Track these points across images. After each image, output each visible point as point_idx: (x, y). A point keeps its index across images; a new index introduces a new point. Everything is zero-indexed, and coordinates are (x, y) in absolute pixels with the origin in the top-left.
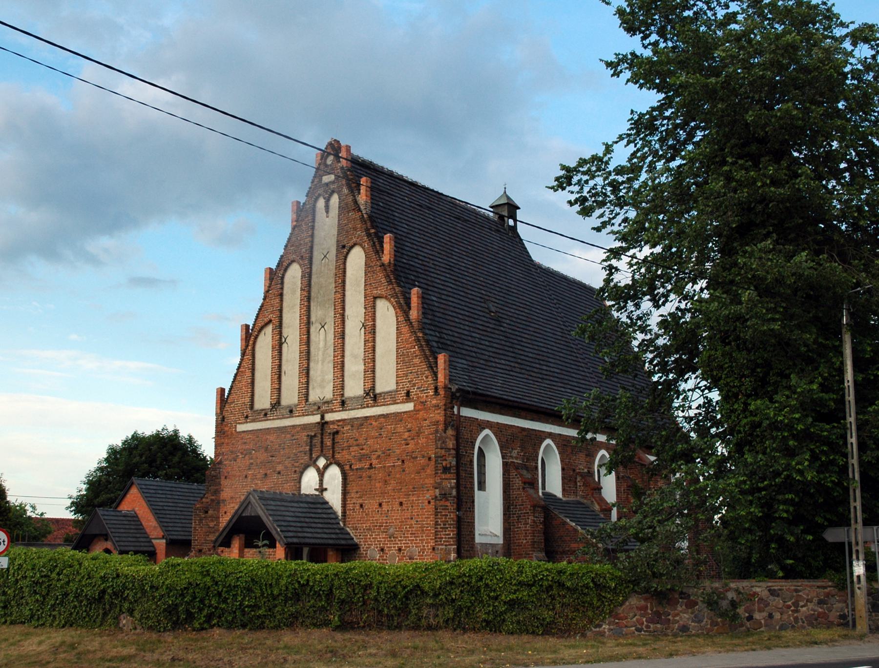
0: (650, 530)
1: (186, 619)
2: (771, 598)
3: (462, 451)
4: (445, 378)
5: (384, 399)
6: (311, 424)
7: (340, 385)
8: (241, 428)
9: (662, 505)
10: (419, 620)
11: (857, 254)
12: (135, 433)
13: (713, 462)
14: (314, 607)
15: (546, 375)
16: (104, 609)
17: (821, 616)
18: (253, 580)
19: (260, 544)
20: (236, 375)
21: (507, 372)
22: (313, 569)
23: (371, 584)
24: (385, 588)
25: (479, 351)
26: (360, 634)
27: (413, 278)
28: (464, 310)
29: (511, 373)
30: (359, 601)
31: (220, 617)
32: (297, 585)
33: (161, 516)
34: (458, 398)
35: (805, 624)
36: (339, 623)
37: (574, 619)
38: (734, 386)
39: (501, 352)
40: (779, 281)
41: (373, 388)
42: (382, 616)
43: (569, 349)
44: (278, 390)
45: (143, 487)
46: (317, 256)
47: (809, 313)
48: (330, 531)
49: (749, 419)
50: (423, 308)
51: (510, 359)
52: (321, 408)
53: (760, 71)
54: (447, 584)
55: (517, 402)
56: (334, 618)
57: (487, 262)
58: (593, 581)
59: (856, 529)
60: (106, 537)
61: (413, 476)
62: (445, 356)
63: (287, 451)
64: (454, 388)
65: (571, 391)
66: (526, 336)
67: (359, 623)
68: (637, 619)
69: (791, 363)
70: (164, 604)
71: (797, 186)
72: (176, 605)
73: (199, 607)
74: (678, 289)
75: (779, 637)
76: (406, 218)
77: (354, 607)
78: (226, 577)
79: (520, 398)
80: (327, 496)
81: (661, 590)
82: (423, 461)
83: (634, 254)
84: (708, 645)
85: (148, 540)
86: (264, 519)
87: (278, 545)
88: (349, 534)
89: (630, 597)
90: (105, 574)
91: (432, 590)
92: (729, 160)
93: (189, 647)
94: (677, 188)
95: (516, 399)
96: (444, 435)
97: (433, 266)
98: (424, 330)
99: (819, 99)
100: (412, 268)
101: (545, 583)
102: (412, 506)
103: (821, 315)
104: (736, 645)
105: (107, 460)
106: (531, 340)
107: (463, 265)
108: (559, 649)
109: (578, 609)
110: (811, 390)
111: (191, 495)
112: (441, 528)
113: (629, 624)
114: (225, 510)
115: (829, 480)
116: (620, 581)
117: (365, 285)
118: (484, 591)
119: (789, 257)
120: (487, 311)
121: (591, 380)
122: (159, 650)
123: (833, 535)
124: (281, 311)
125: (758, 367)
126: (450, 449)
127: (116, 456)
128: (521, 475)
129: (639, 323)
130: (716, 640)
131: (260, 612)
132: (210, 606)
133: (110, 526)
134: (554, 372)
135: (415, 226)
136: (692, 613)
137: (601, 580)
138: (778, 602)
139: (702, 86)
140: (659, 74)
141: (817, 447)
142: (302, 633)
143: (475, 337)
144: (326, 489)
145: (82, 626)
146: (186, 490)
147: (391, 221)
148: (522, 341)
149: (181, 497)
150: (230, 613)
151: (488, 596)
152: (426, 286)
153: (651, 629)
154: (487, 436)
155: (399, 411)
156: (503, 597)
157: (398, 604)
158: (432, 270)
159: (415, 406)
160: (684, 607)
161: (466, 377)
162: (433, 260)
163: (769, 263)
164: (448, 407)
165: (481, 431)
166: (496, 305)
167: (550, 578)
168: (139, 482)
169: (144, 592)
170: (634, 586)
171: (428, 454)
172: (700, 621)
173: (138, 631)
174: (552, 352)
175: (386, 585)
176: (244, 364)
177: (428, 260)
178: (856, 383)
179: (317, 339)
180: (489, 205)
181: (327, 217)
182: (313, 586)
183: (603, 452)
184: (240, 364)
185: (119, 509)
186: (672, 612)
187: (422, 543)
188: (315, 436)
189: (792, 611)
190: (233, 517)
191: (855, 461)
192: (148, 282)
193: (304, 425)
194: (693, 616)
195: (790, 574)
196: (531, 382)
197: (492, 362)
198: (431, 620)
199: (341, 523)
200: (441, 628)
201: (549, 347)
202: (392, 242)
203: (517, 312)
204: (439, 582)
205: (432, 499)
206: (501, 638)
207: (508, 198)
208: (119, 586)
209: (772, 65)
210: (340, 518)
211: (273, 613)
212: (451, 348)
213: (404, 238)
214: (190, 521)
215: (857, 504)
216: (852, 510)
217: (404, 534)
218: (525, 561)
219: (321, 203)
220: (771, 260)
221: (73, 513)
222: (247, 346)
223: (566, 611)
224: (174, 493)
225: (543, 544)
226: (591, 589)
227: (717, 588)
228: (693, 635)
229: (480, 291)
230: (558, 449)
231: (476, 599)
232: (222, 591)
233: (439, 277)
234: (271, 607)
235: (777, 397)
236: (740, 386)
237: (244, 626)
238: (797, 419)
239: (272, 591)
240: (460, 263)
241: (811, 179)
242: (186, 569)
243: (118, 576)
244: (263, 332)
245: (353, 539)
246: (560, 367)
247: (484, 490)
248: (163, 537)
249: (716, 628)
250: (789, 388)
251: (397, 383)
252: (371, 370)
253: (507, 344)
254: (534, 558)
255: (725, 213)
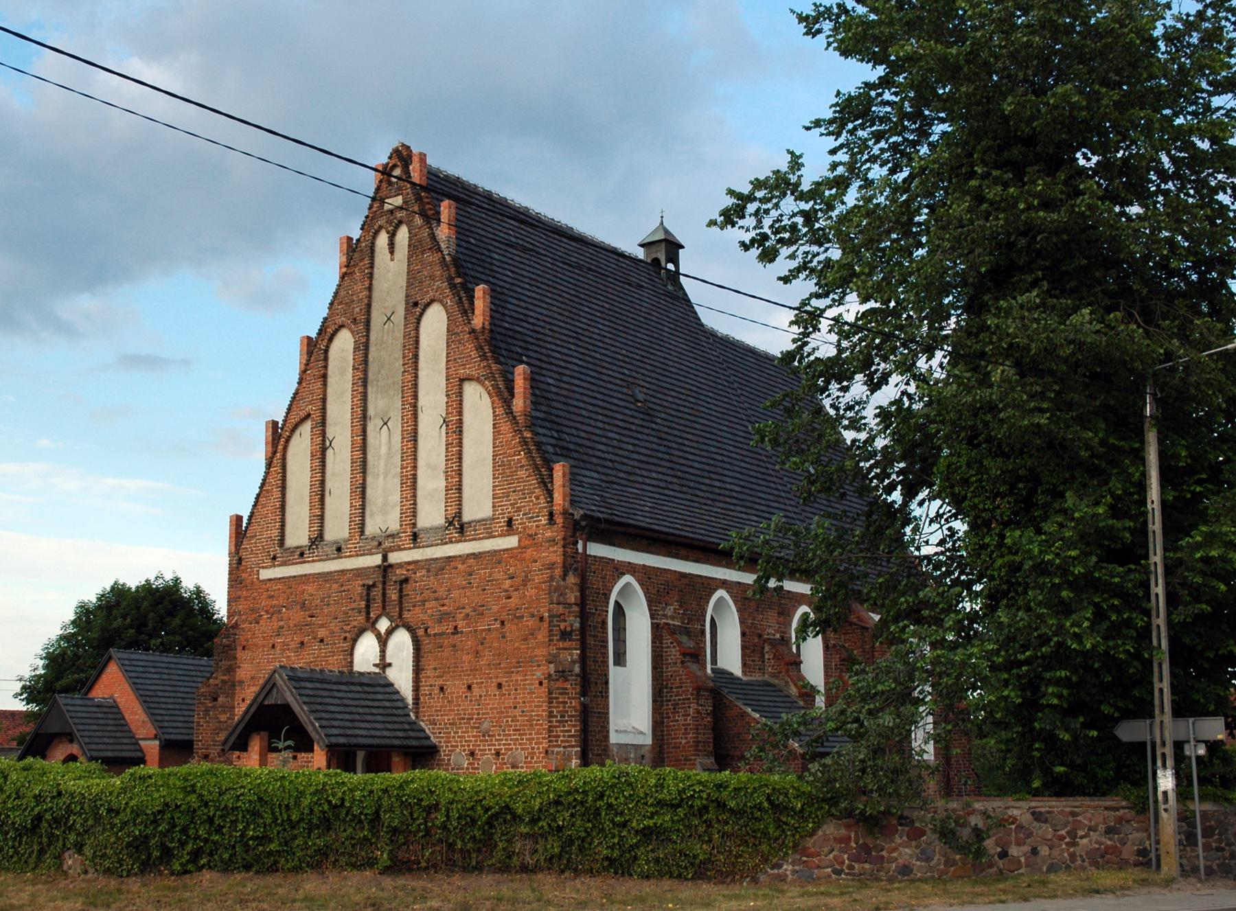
0: (855, 725)
1: (161, 857)
2: (1036, 824)
3: (590, 608)
4: (564, 500)
5: (475, 530)
6: (369, 568)
7: (411, 510)
8: (265, 574)
9: (875, 687)
10: (509, 857)
11: (1169, 311)
12: (116, 583)
13: (951, 623)
14: (352, 838)
15: (719, 495)
16: (40, 843)
17: (1110, 851)
18: (260, 799)
19: (281, 746)
20: (258, 496)
21: (661, 491)
22: (351, 783)
23: (437, 804)
24: (458, 810)
25: (617, 458)
26: (419, 879)
27: (519, 350)
28: (596, 398)
29: (667, 492)
30: (419, 830)
31: (211, 854)
32: (326, 807)
33: (152, 705)
34: (583, 528)
35: (1086, 864)
36: (389, 863)
37: (741, 856)
38: (985, 510)
39: (651, 460)
40: (1050, 351)
41: (459, 514)
42: (454, 851)
43: (756, 456)
44: (319, 518)
45: (127, 662)
46: (377, 317)
47: (1096, 398)
48: (396, 726)
49: (1006, 559)
50: (534, 394)
51: (664, 470)
52: (383, 544)
53: (1024, 36)
54: (550, 804)
55: (673, 535)
56: (382, 855)
57: (632, 327)
58: (768, 799)
59: (1162, 722)
60: (70, 738)
61: (516, 644)
62: (563, 466)
63: (332, 608)
64: (578, 514)
65: (755, 518)
66: (690, 437)
67: (419, 863)
68: (834, 856)
69: (1067, 476)
70: (128, 836)
71: (1077, 210)
72: (146, 837)
73: (179, 840)
74: (906, 367)
75: (1044, 883)
76: (510, 262)
77: (412, 838)
78: (220, 795)
79: (678, 529)
80: (391, 674)
81: (871, 814)
82: (531, 623)
83: (840, 315)
84: (936, 894)
85: (134, 741)
86: (296, 708)
87: (316, 747)
88: (423, 730)
89: (824, 823)
90: (41, 791)
91: (528, 813)
92: (978, 169)
93: (161, 899)
94: (903, 214)
95: (671, 531)
96: (562, 583)
97: (550, 333)
98: (534, 428)
99: (1114, 78)
100: (518, 336)
101: (698, 802)
102: (516, 690)
103: (1112, 403)
104: (977, 895)
105: (73, 622)
106: (697, 442)
107: (596, 331)
108: (715, 900)
109: (746, 842)
110: (1096, 515)
111: (199, 674)
112: (557, 721)
113: (823, 865)
114: (243, 696)
115: (1121, 649)
116: (810, 799)
117: (447, 362)
118: (606, 814)
119: (1066, 314)
120: (631, 399)
121: (788, 502)
122: (118, 904)
123: (1128, 732)
124: (324, 400)
125: (1021, 481)
126: (570, 605)
127: (88, 618)
128: (679, 643)
129: (850, 414)
130: (950, 887)
131: (272, 846)
132: (197, 838)
133: (76, 721)
134: (731, 490)
135: (524, 273)
136: (917, 847)
137: (781, 798)
138: (1046, 830)
139: (938, 60)
140: (876, 40)
141: (1104, 600)
142: (333, 878)
143: (612, 439)
144: (390, 665)
145: (8, 870)
146: (191, 667)
147: (487, 266)
148: (684, 445)
149: (182, 678)
150: (226, 848)
151: (612, 821)
152: (538, 363)
153: (856, 871)
154: (628, 584)
155: (496, 548)
156: (634, 824)
157: (478, 834)
158: (549, 339)
159: (519, 541)
160: (905, 838)
161: (596, 498)
162: (550, 324)
163: (1035, 326)
164: (569, 542)
165: (619, 578)
166: (645, 390)
167: (704, 795)
168: (120, 655)
169: (98, 818)
170: (830, 808)
171: (539, 611)
172: (928, 859)
173: (90, 876)
174: (729, 460)
175: (459, 806)
176: (270, 480)
177: (542, 324)
178: (1164, 503)
179: (377, 443)
180: (639, 241)
181: (392, 260)
182: (351, 807)
183: (804, 609)
184: (264, 480)
185: (90, 696)
186: (887, 846)
187: (530, 744)
188: (374, 585)
189: (1067, 844)
190: (251, 706)
191: (1160, 621)
192: (150, 363)
193: (357, 569)
194: (918, 851)
195: (1060, 788)
196: (696, 505)
197: (637, 475)
198: (528, 858)
199: (412, 714)
200: (541, 870)
201: (725, 453)
202: (487, 297)
203: (677, 401)
204: (539, 800)
205: (545, 679)
206: (630, 884)
207: (666, 232)
208: (61, 809)
209: (1043, 27)
210: (410, 707)
211: (292, 848)
212: (575, 455)
213: (506, 291)
214: (191, 713)
215: (1163, 685)
216: (1156, 694)
217: (504, 731)
218: (668, 769)
219: (383, 239)
220: (1037, 321)
221: (24, 703)
222: (274, 453)
223: (728, 844)
224: (173, 672)
225: (712, 745)
226: (766, 812)
227: (954, 810)
228: (919, 880)
229: (621, 370)
230: (736, 604)
231: (594, 826)
232: (214, 815)
233: (559, 349)
234: (288, 839)
235: (1046, 527)
236: (994, 509)
237: (247, 867)
238: (1074, 558)
239: (289, 816)
240: (591, 329)
241: (1100, 198)
242: (160, 783)
243: (60, 794)
244: (298, 432)
245: (429, 738)
246: (741, 483)
247: (624, 665)
248: (156, 737)
249: (952, 869)
250: (1064, 512)
251: (494, 507)
252: (455, 489)
253: (662, 449)
254: (698, 766)
255: (971, 251)
